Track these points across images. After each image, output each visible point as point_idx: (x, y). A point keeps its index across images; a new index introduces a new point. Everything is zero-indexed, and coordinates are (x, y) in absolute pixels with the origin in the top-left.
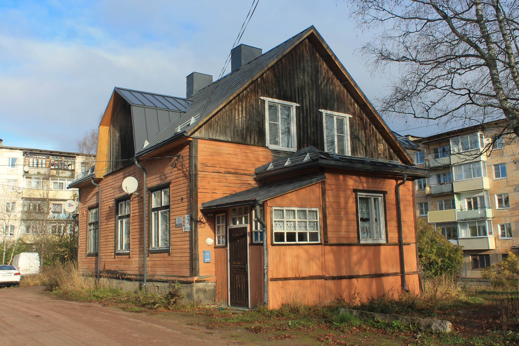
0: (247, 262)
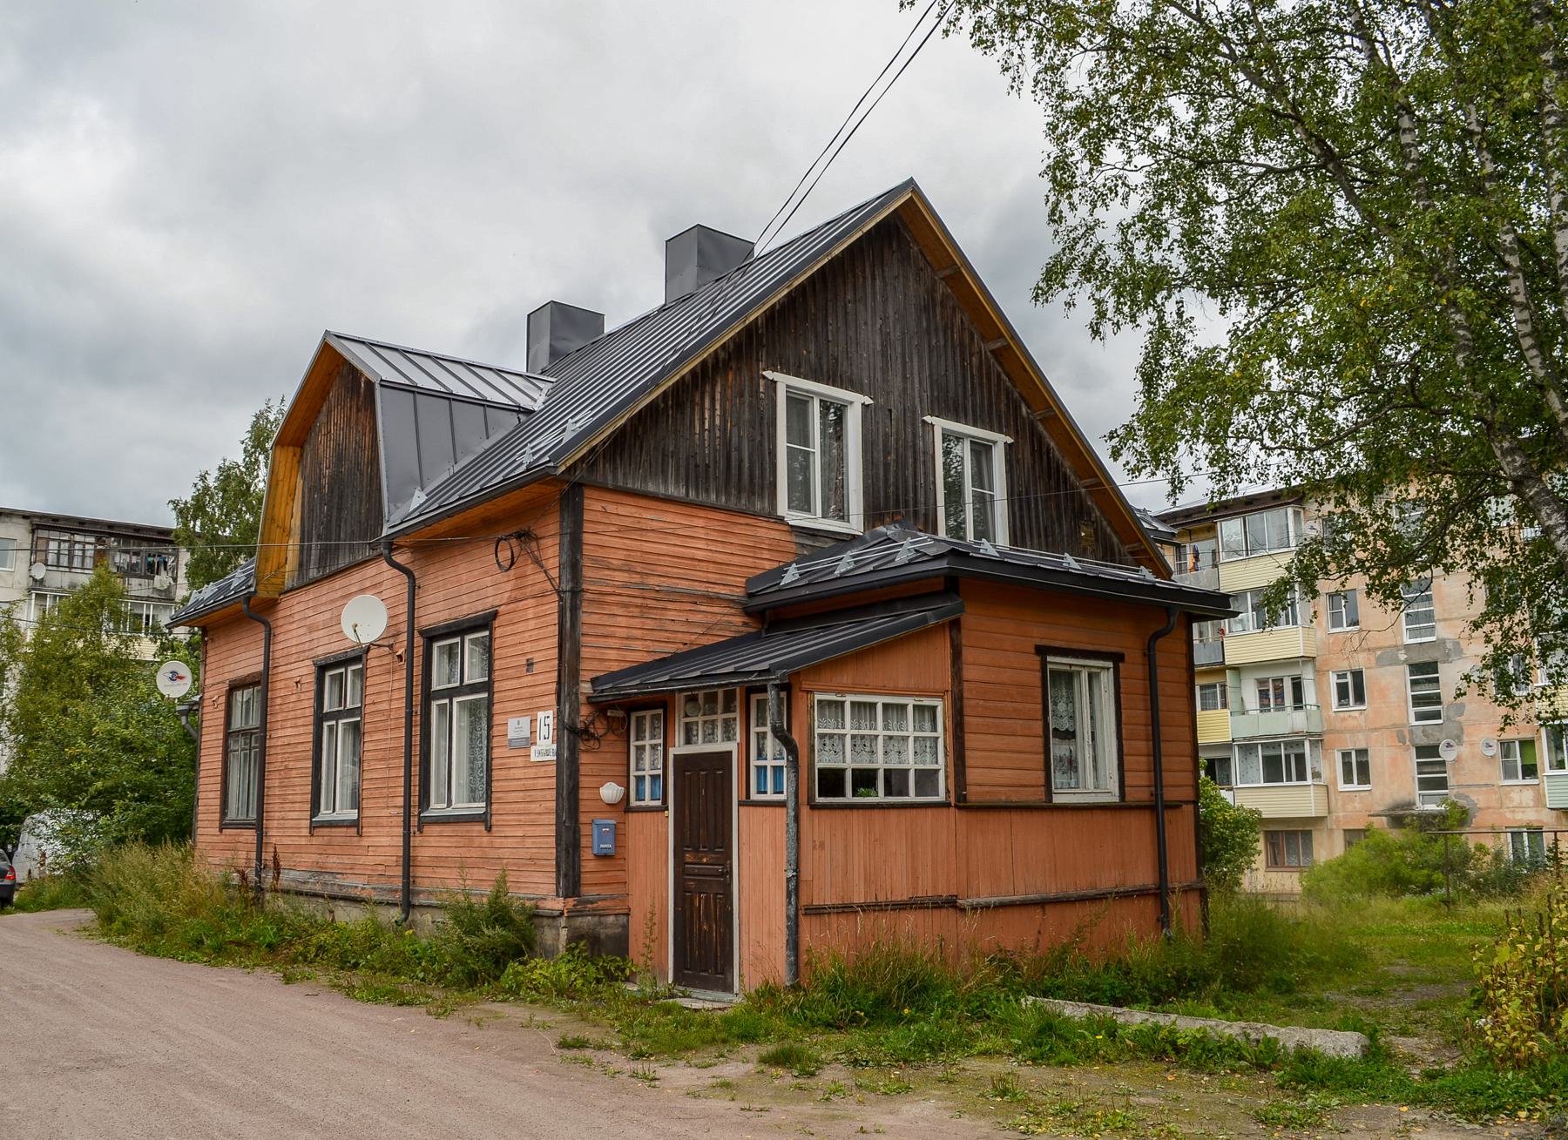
0: (730, 858)
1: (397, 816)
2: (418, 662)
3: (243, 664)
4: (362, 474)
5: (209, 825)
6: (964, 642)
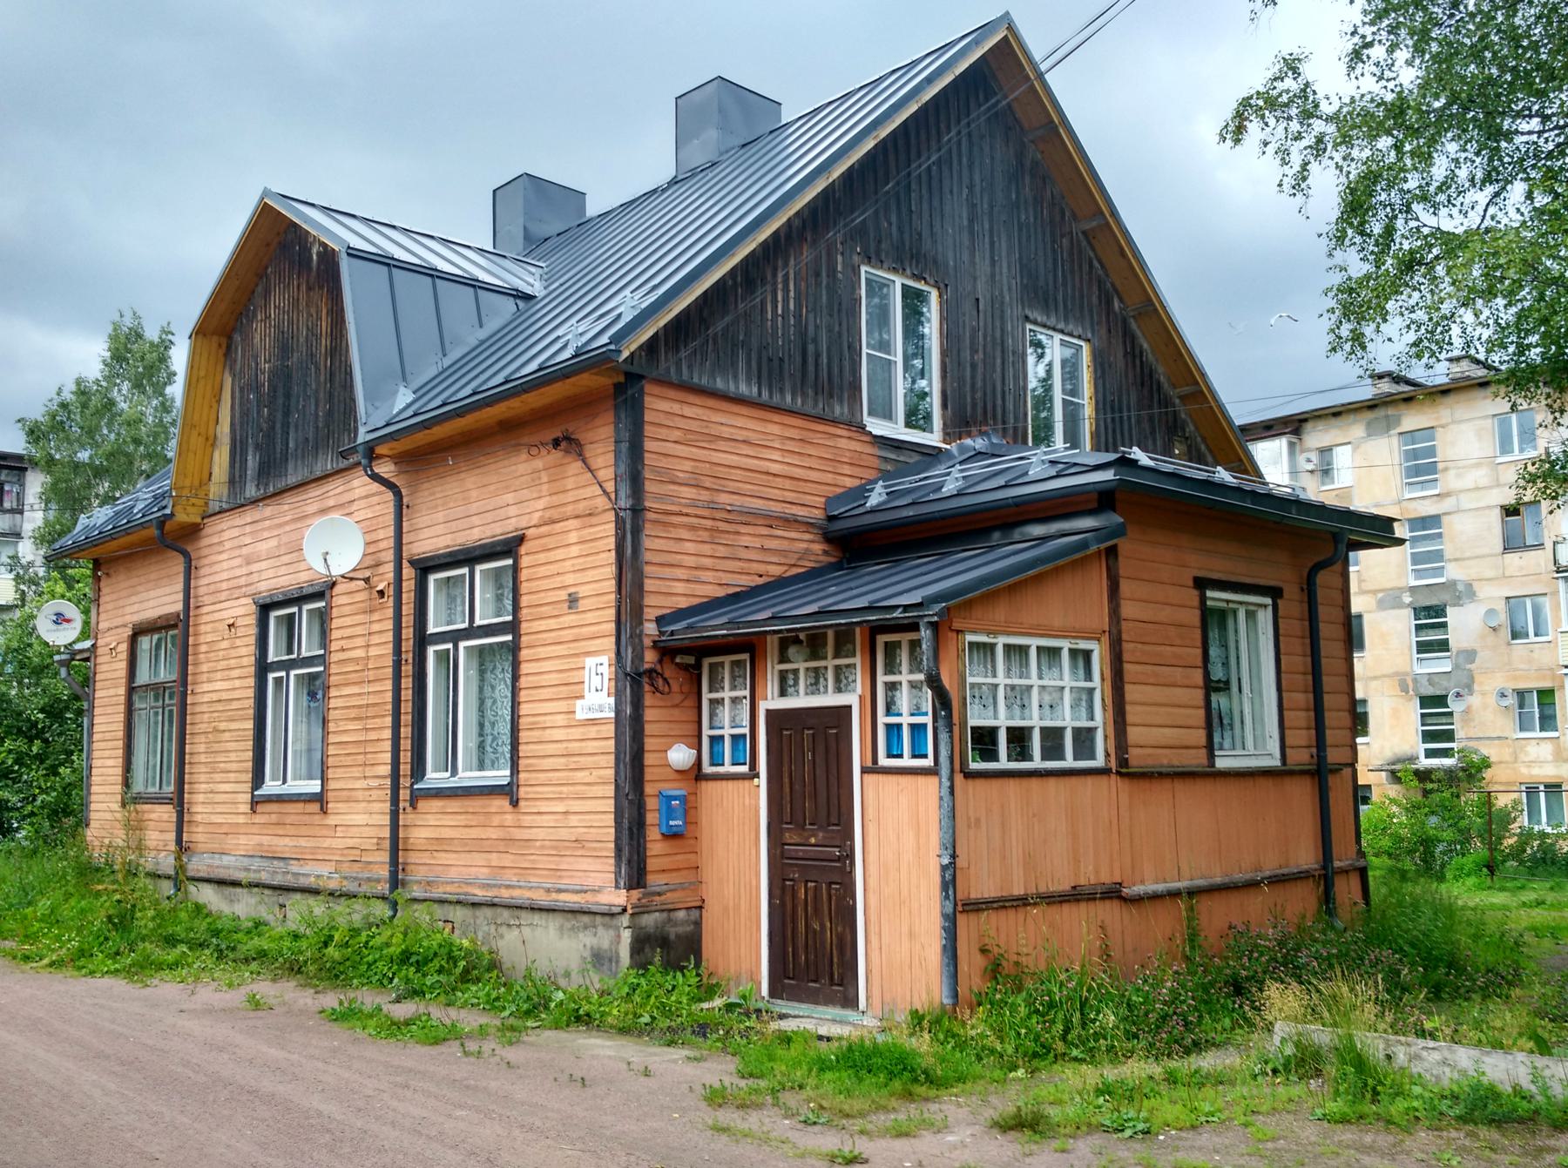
1: (380, 788)
2: (408, 597)
3: (151, 604)
4: (317, 369)
5: (107, 798)
6: (1122, 572)
